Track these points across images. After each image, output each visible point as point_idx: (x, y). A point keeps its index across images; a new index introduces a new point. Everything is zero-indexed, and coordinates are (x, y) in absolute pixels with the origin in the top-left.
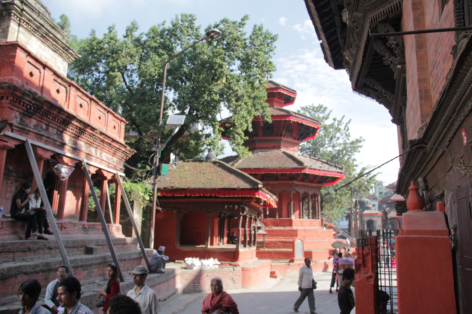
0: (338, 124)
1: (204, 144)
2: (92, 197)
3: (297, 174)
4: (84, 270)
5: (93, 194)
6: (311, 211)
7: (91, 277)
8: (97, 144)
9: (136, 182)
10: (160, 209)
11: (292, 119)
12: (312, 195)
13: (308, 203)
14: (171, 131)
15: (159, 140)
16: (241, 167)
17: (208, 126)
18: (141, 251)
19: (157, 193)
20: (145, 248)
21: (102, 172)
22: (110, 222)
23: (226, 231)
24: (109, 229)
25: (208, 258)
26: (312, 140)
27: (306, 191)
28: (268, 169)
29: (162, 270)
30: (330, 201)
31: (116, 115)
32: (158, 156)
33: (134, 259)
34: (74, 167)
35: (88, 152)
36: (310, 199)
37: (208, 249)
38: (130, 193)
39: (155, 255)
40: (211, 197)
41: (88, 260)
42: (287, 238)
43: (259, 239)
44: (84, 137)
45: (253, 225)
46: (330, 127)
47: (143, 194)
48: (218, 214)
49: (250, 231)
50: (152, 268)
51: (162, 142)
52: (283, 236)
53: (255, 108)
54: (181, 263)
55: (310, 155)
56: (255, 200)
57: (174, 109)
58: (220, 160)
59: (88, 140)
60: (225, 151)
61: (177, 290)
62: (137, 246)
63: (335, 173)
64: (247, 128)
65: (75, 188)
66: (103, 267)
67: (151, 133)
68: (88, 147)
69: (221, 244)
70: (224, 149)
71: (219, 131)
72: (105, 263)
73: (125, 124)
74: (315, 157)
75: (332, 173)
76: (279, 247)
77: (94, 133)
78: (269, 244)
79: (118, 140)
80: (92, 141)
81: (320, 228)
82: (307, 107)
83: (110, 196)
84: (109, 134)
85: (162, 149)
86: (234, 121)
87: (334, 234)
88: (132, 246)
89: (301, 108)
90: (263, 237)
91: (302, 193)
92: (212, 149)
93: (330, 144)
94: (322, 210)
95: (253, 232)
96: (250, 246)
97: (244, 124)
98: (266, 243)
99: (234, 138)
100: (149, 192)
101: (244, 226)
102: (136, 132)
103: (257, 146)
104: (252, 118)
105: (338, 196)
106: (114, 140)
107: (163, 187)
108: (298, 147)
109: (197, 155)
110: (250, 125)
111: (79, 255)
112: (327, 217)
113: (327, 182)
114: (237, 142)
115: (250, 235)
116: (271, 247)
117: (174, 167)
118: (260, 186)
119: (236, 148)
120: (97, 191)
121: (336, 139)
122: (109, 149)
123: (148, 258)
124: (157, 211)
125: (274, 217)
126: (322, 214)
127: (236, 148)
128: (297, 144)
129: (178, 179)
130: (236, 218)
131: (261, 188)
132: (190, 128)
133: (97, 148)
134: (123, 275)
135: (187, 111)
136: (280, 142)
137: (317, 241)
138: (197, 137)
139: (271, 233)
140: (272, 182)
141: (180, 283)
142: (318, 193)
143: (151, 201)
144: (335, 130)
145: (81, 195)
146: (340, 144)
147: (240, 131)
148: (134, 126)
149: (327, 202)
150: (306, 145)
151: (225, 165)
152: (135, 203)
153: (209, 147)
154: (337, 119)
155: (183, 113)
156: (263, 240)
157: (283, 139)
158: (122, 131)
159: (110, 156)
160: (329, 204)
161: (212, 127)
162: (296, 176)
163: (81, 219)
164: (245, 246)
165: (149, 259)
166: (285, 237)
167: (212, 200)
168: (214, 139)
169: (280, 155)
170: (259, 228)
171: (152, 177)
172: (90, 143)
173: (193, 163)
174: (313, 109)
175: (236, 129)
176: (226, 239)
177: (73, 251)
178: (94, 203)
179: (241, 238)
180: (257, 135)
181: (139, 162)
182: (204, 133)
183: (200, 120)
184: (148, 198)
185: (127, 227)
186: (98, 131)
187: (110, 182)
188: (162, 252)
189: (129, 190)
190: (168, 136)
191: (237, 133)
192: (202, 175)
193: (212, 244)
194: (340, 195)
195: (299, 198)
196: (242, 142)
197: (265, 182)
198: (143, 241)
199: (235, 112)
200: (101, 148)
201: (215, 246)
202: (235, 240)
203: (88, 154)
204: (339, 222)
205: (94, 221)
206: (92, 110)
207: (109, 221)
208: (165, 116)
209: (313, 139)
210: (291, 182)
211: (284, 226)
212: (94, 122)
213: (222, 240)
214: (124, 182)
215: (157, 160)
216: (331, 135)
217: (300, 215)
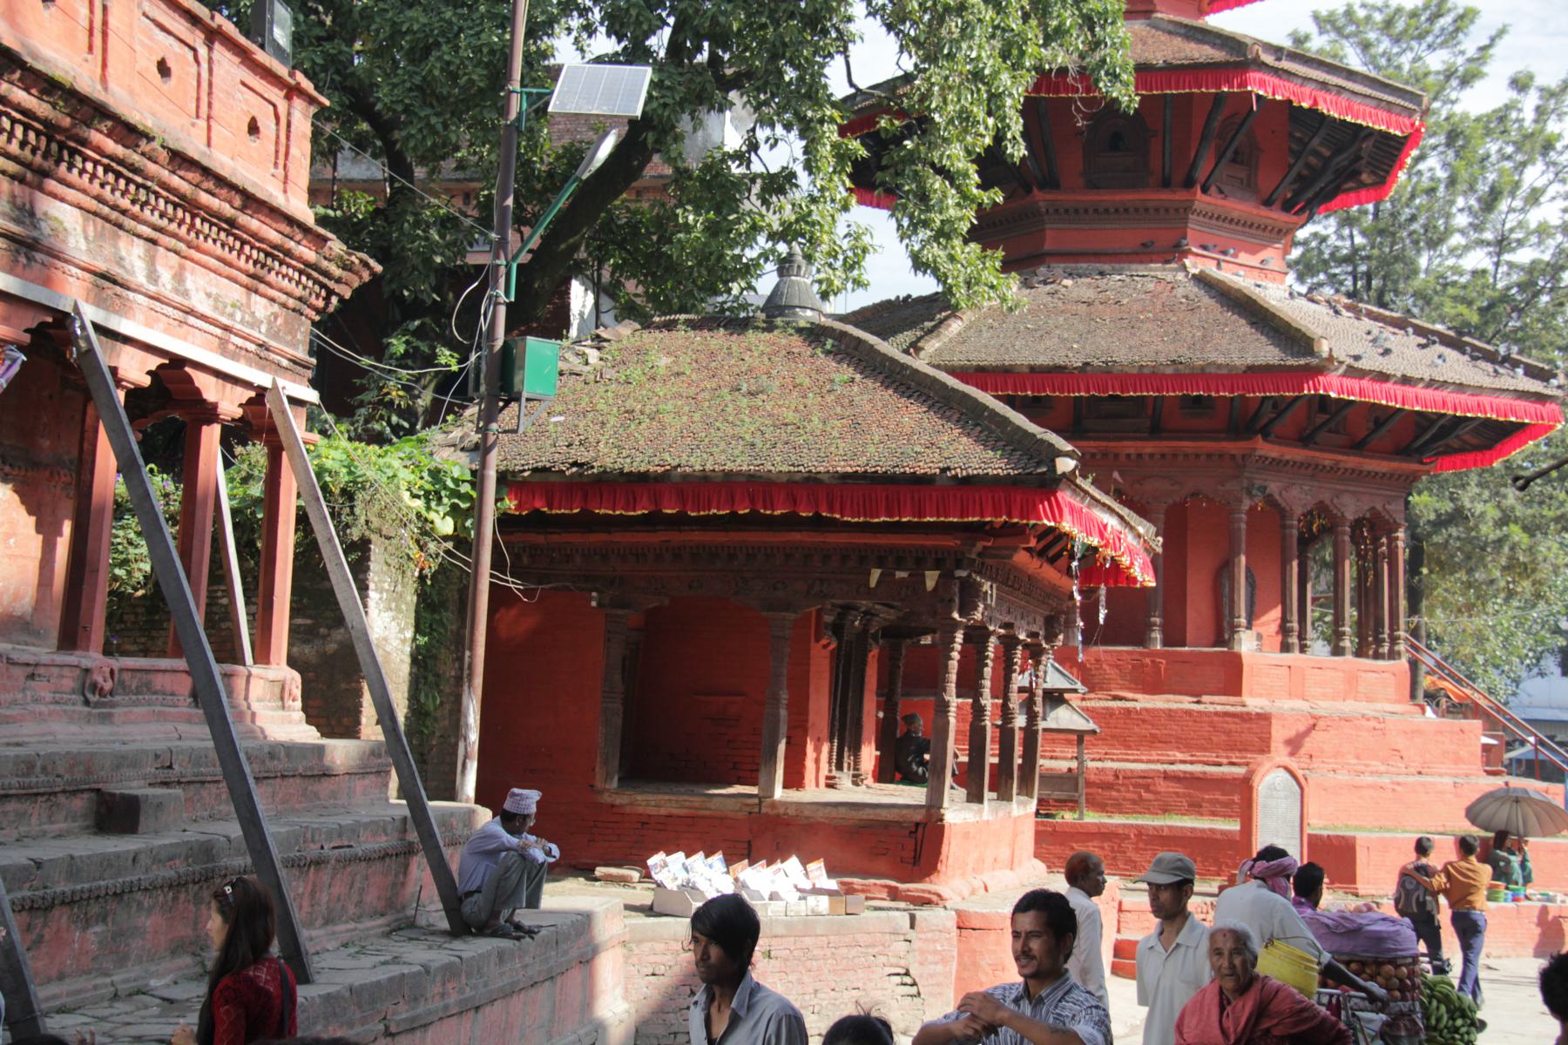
0: (1541, 112)
1: (755, 228)
2: (132, 521)
3: (1276, 402)
4: (87, 924)
5: (139, 503)
6: (1350, 613)
7: (122, 961)
8: (155, 219)
9: (379, 439)
10: (514, 584)
11: (1259, 86)
12: (1357, 525)
13: (1336, 566)
14: (574, 156)
15: (510, 202)
16: (958, 359)
17: (779, 130)
18: (407, 812)
19: (498, 500)
20: (430, 799)
21: (190, 380)
22: (235, 657)
23: (871, 713)
24: (230, 694)
25: (775, 854)
26: (1370, 207)
27: (1326, 496)
28: (1108, 374)
29: (524, 917)
30: (1468, 557)
31: (261, 56)
32: (503, 293)
33: (367, 859)
34: (21, 348)
35: (102, 266)
36: (1349, 547)
37: (774, 805)
38: (348, 494)
39: (487, 836)
40: (791, 522)
41: (107, 863)
42: (1212, 757)
43: (1054, 762)
44: (74, 176)
45: (1020, 680)
46: (1488, 132)
47: (419, 504)
48: (828, 619)
49: (1006, 713)
50: (468, 907)
51: (521, 220)
52: (1185, 744)
53: (1043, 25)
54: (624, 881)
55: (1351, 295)
56: (1033, 543)
57: (589, 29)
58: (843, 318)
59: (99, 199)
60: (871, 267)
61: (599, 1028)
62: (386, 785)
63: (1505, 401)
64: (999, 138)
65: (36, 465)
66: (198, 901)
67: (461, 165)
68: (100, 236)
69: (845, 779)
70: (869, 261)
71: (841, 156)
72: (206, 878)
73: (313, 110)
74: (1383, 305)
75: (1485, 400)
76: (1166, 810)
77: (135, 158)
78: (1108, 786)
79: (279, 200)
80: (125, 203)
81: (1407, 707)
82: (1349, 13)
83: (234, 512)
84: (222, 161)
85: (525, 258)
86: (924, 98)
87: (1486, 748)
88: (359, 784)
89: (1316, 17)
90: (1072, 751)
91: (1299, 511)
92: (799, 258)
93: (1477, 228)
94: (1414, 609)
95: (1020, 721)
96: (1005, 796)
97: (981, 111)
98: (1089, 784)
99: (923, 197)
100: (455, 494)
101: (969, 685)
102: (375, 156)
103: (1048, 246)
104: (1029, 79)
105: (1516, 533)
106: (251, 202)
107: (532, 464)
108: (1286, 252)
109: (716, 293)
110: (1016, 126)
111: (59, 836)
112: (1447, 649)
113: (1450, 451)
114: (937, 219)
115: (1006, 734)
116: (1118, 808)
117: (593, 355)
118: (1065, 465)
119: (935, 252)
120: (160, 484)
121: (1518, 204)
122: (225, 254)
123: (447, 852)
124: (499, 596)
125: (1141, 639)
126: (1415, 632)
127: (935, 252)
128: (1282, 234)
129: (613, 421)
130: (927, 640)
131: (1069, 478)
132: (678, 138)
133: (154, 242)
134: (308, 946)
135: (659, 42)
136: (1185, 220)
137: (1385, 780)
138: (717, 188)
139: (1117, 730)
140: (1130, 447)
141: (619, 991)
142: (1396, 508)
143: (463, 543)
144: (1519, 147)
145: (68, 505)
146: (1543, 231)
147: (956, 156)
148: (365, 126)
149: (1446, 567)
150: (1333, 240)
151: (869, 345)
152: (377, 551)
153: (782, 248)
154: (1540, 81)
155: (636, 54)
156: (1074, 765)
157: (1201, 201)
158: (294, 151)
159: (236, 293)
160: (1462, 575)
161: (802, 136)
162: (1268, 413)
163: (70, 637)
164: (976, 797)
165: (455, 859)
166: (1200, 755)
167: (796, 537)
168: (813, 200)
169: (1180, 292)
170: (1055, 698)
171: (472, 411)
172: (114, 215)
173: (697, 337)
174: (1388, 24)
175: (931, 146)
176: (869, 755)
177: (21, 816)
178: (144, 550)
179: (956, 752)
180: (1051, 182)
181: (395, 328)
182: (757, 167)
183: (733, 95)
184: (446, 526)
185: (333, 685)
186: (156, 144)
187: (235, 434)
188: (525, 817)
189: (344, 477)
190: (554, 181)
191: (942, 171)
192: (744, 402)
193: (794, 779)
194: (1529, 530)
195: (1284, 538)
196: (966, 218)
197: (1091, 445)
198: (422, 760)
199: (930, 49)
200: (182, 246)
201: (812, 793)
202: (923, 763)
203: (104, 276)
204: (1517, 681)
205: (145, 653)
206: (112, 21)
207: (229, 652)
208: (542, 73)
209: (1378, 201)
210: (1234, 447)
211: (1197, 694)
212: (131, 92)
213: (847, 760)
214: (315, 436)
215: (496, 319)
216: (1491, 177)
217: (1284, 630)
